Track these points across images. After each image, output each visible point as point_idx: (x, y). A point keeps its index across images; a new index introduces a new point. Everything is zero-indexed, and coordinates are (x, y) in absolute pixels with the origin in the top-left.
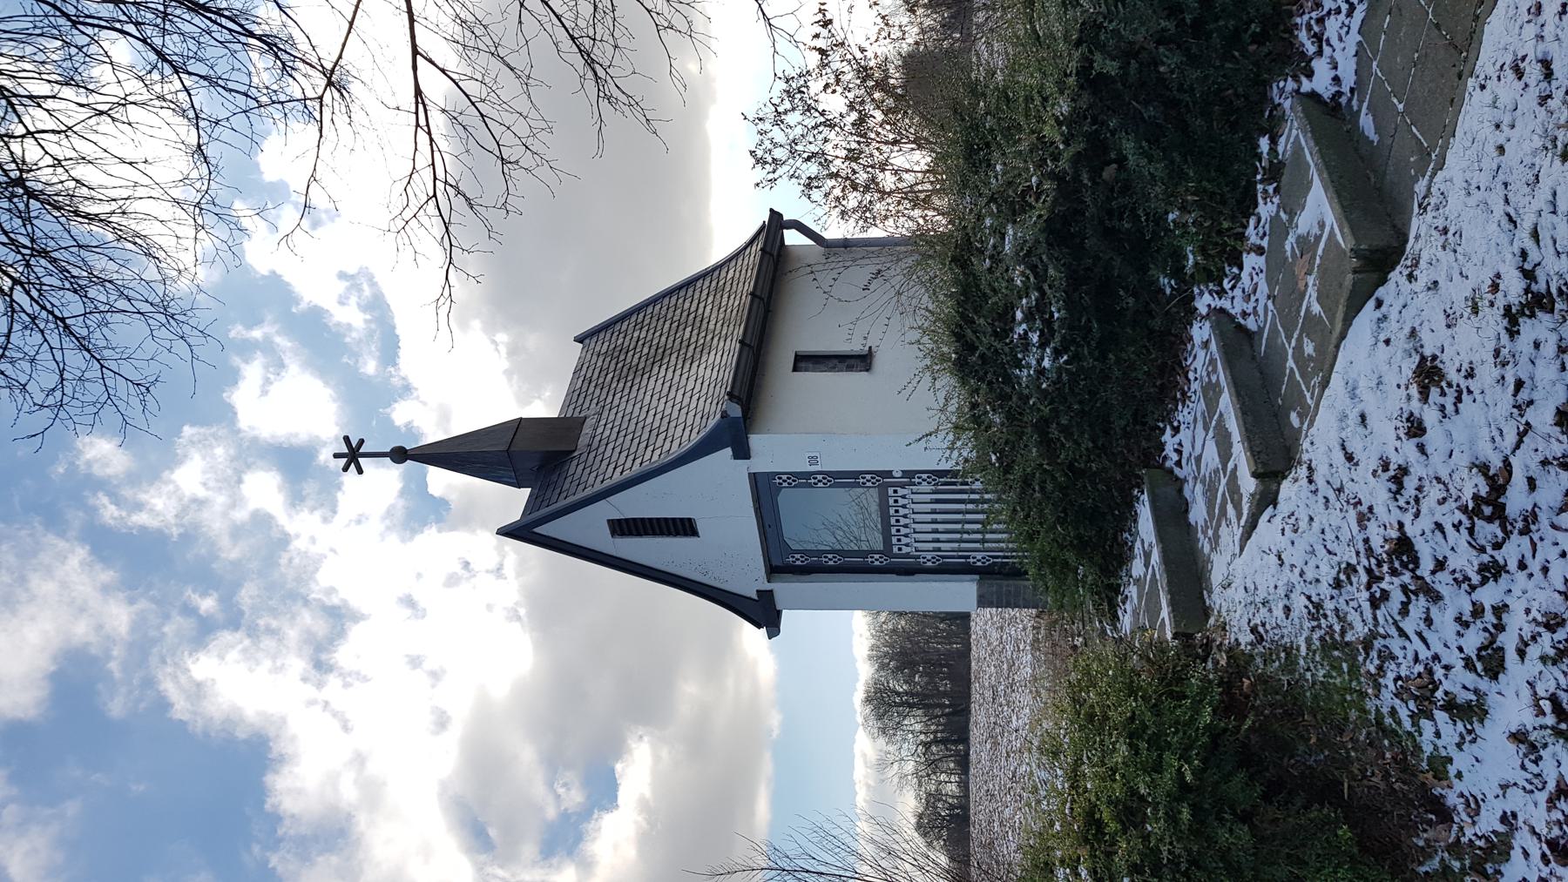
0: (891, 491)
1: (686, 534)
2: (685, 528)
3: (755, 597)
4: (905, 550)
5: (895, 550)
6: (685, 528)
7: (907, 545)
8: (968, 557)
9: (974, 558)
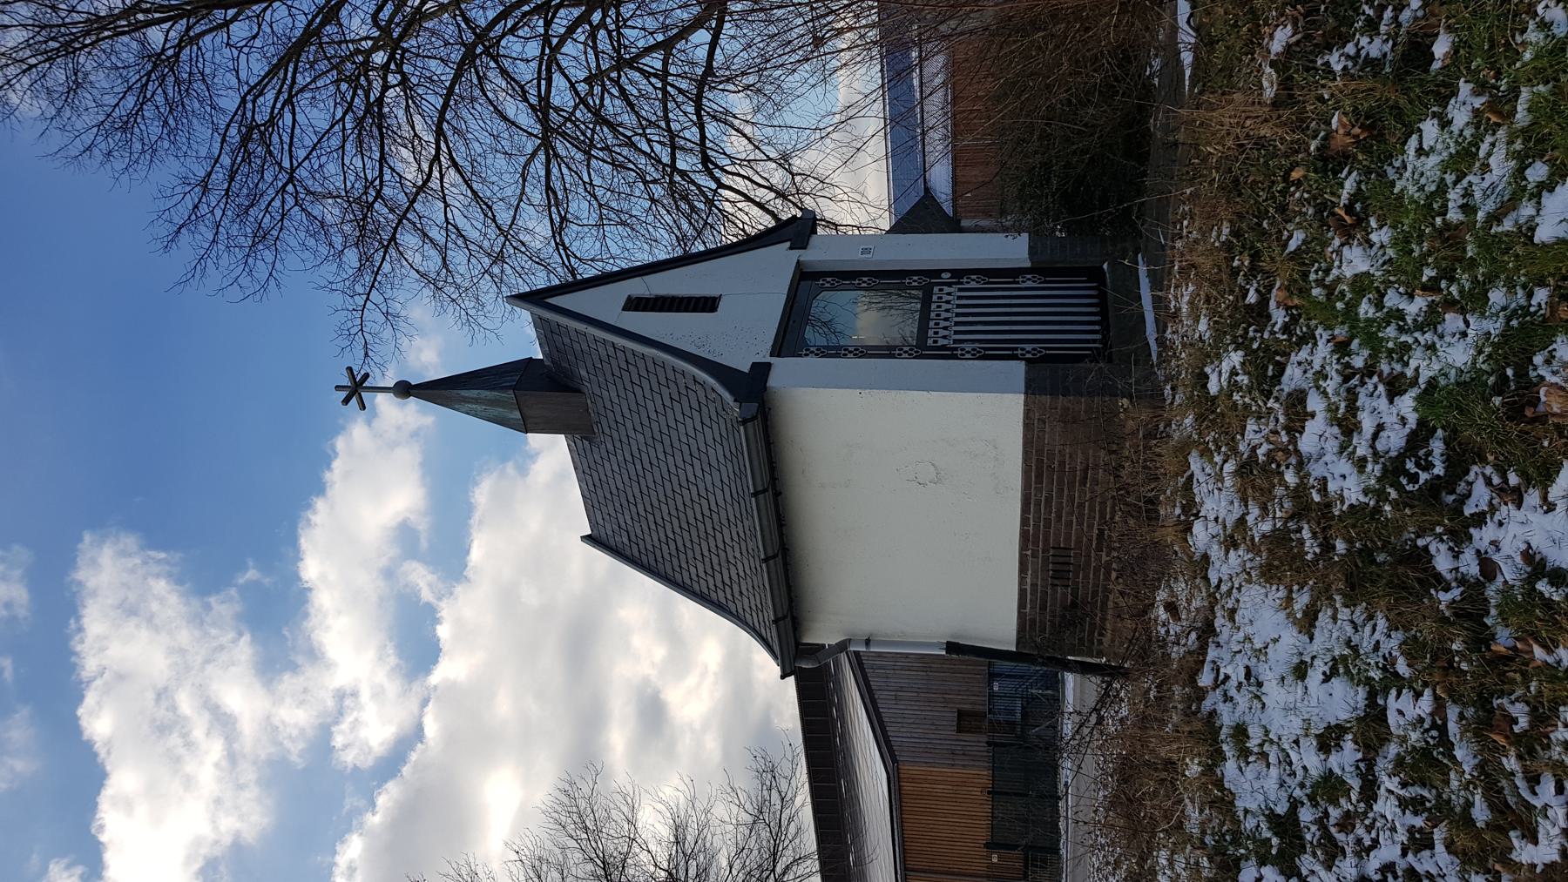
0: (936, 289)
1: (769, 370)
2: (708, 304)
3: (746, 369)
4: (941, 342)
5: (930, 342)
6: (708, 304)
7: (944, 337)
8: (1016, 349)
9: (1023, 349)
